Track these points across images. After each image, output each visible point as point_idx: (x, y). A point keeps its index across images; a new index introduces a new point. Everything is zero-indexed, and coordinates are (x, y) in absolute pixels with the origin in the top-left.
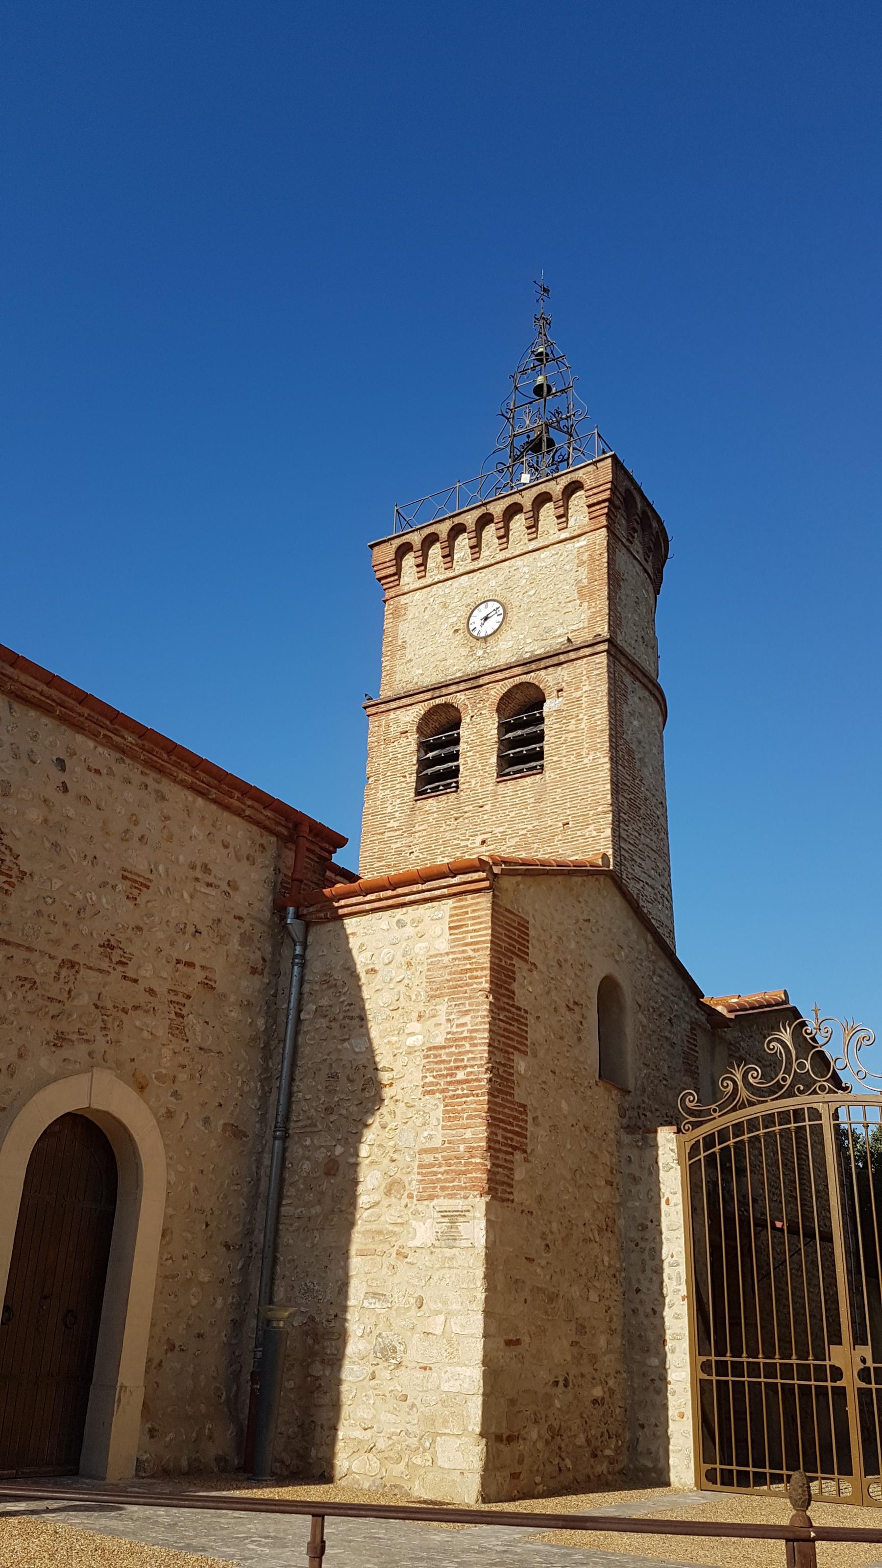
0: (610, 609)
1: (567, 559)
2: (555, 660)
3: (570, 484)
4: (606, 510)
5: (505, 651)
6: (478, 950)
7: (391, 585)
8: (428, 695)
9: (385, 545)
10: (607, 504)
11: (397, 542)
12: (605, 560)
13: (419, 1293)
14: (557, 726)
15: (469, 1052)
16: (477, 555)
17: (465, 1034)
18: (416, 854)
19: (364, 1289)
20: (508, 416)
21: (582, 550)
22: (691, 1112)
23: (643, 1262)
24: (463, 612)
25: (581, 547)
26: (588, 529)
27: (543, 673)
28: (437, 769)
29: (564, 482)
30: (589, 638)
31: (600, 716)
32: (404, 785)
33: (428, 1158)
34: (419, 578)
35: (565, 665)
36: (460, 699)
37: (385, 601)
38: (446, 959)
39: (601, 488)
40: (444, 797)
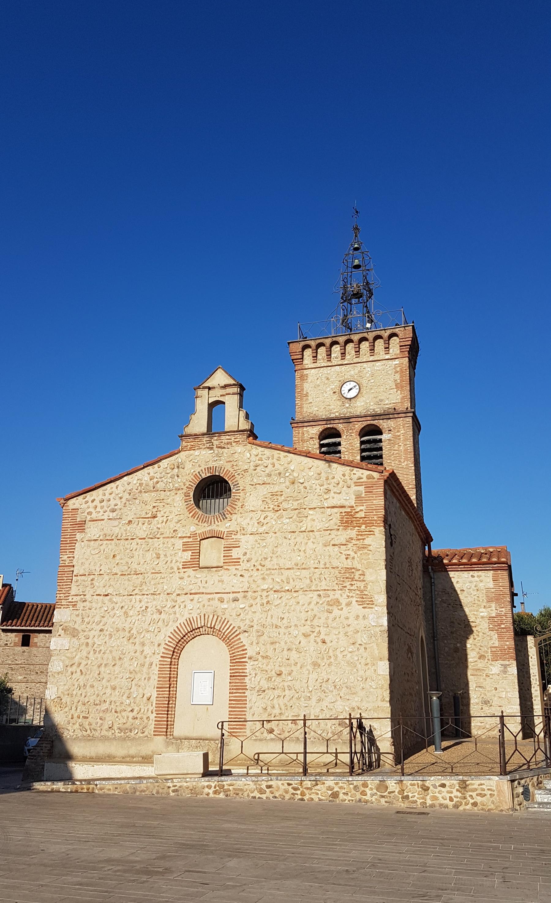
4: (408, 350)
5: (360, 407)
8: (324, 422)
11: (303, 344)
12: (408, 373)
13: (495, 686)
19: (475, 685)
22: (540, 632)
23: (524, 675)
24: (337, 384)
26: (399, 356)
27: (381, 421)
29: (388, 332)
33: (494, 649)
36: (340, 427)
37: (295, 371)
38: (493, 590)
39: (407, 339)
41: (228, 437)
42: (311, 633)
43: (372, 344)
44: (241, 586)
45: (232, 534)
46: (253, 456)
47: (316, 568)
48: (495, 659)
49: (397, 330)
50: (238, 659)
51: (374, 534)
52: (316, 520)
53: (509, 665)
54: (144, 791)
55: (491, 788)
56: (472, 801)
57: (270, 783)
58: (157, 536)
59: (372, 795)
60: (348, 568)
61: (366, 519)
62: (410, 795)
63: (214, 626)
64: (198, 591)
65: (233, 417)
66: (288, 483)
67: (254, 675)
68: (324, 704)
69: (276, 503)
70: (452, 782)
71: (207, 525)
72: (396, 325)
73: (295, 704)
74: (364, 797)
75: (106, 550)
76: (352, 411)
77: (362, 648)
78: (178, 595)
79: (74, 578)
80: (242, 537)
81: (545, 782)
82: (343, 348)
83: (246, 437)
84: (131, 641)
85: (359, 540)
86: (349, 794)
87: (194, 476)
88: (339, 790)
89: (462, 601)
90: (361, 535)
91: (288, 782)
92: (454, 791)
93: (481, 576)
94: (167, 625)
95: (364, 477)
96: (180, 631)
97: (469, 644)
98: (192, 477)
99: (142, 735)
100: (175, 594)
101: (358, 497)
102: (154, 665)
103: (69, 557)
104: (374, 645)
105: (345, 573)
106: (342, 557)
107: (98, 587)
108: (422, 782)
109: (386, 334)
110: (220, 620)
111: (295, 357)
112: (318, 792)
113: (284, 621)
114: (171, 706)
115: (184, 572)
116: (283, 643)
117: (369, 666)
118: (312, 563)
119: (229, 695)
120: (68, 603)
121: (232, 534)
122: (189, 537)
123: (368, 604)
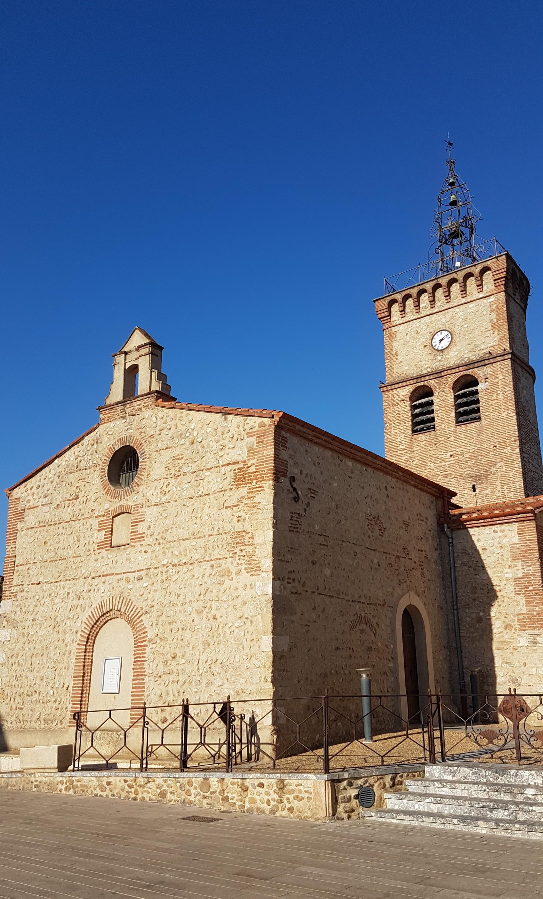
0: (509, 335)
1: (484, 308)
2: (483, 363)
3: (483, 268)
4: (504, 282)
5: (453, 357)
6: (532, 543)
7: (386, 321)
8: (414, 381)
9: (381, 300)
10: (504, 279)
11: (388, 299)
12: (505, 309)
13: (524, 661)
14: (486, 397)
15: (533, 580)
16: (433, 306)
17: (531, 573)
18: (416, 462)
19: (501, 661)
20: (440, 221)
21: (492, 303)
24: (428, 336)
25: (492, 302)
26: (494, 292)
27: (476, 369)
28: (422, 420)
29: (480, 267)
30: (501, 352)
31: (509, 392)
32: (405, 427)
34: (402, 318)
35: (488, 366)
36: (432, 383)
37: (383, 330)
38: (518, 546)
39: (501, 271)
40: (428, 434)
41: (138, 403)
42: (203, 609)
43: (463, 284)
44: (145, 563)
45: (138, 507)
46: (159, 419)
47: (210, 536)
48: (523, 629)
49: (489, 262)
50: (139, 642)
51: (263, 490)
52: (213, 481)
53: (539, 635)
54: (14, 786)
55: (309, 789)
56: (288, 806)
57: (110, 779)
58: (79, 518)
59: (196, 795)
60: (239, 532)
61: (257, 473)
62: (230, 796)
63: (120, 608)
64: (110, 573)
65: (146, 380)
66: (188, 444)
67: (152, 660)
68: (214, 687)
69: (177, 468)
70: (270, 780)
71: (117, 501)
72: (490, 257)
73: (187, 689)
74: (189, 797)
75: (40, 537)
76: (445, 363)
77: (248, 622)
78: (93, 578)
79: (16, 568)
80: (147, 509)
81: (407, 782)
82: (431, 295)
83: (153, 400)
84: (55, 629)
85: (249, 498)
86: (176, 793)
87: (109, 450)
88: (167, 788)
89: (485, 562)
90: (252, 492)
91: (124, 778)
92: (272, 792)
93: (504, 531)
94: (84, 611)
95: (256, 425)
96: (93, 616)
97: (494, 612)
98: (108, 450)
99: (60, 726)
100: (90, 578)
101: (250, 450)
102: (72, 653)
103: (12, 548)
104: (259, 617)
105: (236, 537)
106: (234, 520)
107: (33, 576)
108: (242, 781)
109: (477, 270)
110: (126, 602)
111: (382, 315)
112: (149, 790)
113: (181, 598)
114: (84, 695)
115: (99, 553)
116: (179, 622)
117: (254, 642)
118: (206, 531)
119: (132, 682)
120: (10, 594)
121: (138, 507)
122: (104, 516)
123: (256, 571)
